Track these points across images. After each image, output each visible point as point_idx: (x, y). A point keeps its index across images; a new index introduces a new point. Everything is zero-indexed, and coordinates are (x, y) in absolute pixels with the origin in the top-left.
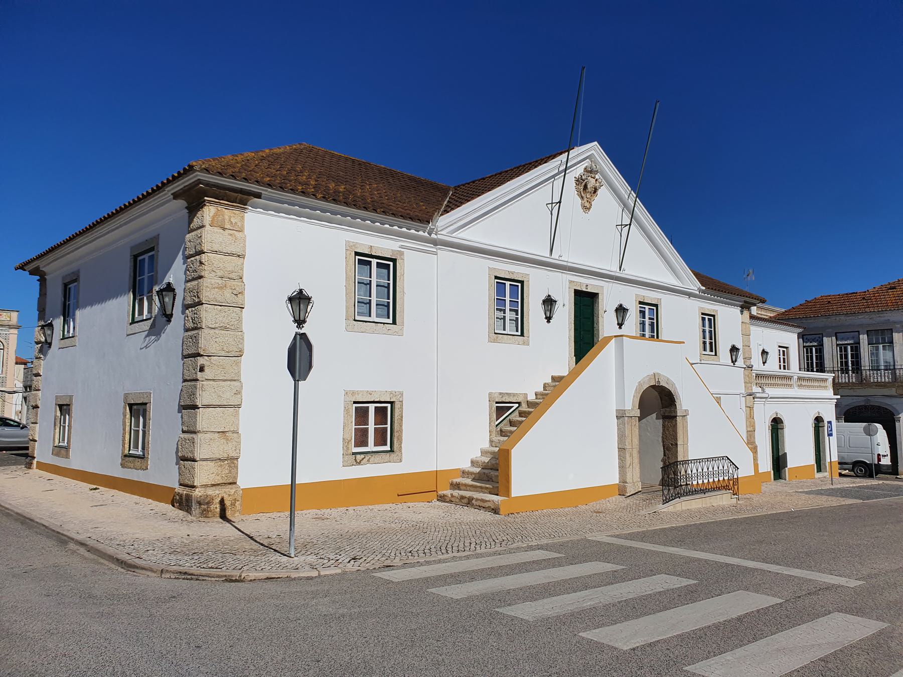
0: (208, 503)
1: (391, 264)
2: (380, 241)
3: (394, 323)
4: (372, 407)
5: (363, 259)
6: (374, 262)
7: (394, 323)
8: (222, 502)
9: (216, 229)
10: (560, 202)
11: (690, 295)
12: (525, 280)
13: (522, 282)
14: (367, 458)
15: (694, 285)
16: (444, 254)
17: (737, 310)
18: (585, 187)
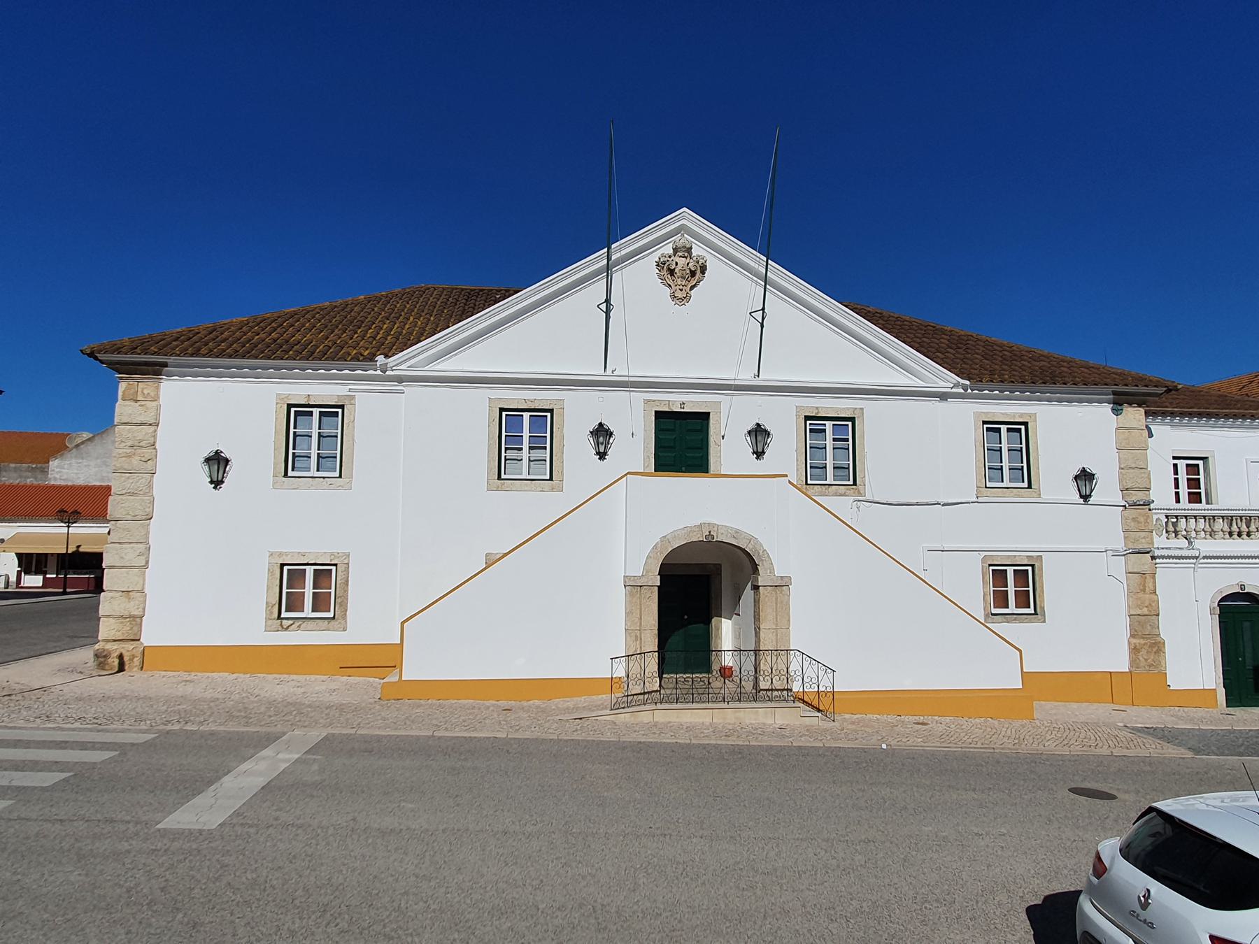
0: (105, 656)
1: (1023, 427)
3: (1030, 486)
4: (1010, 570)
5: (992, 427)
6: (1004, 428)
7: (1030, 486)
8: (121, 657)
9: (128, 403)
10: (763, 309)
11: (943, 397)
12: (555, 407)
14: (297, 624)
15: (946, 379)
18: (672, 272)
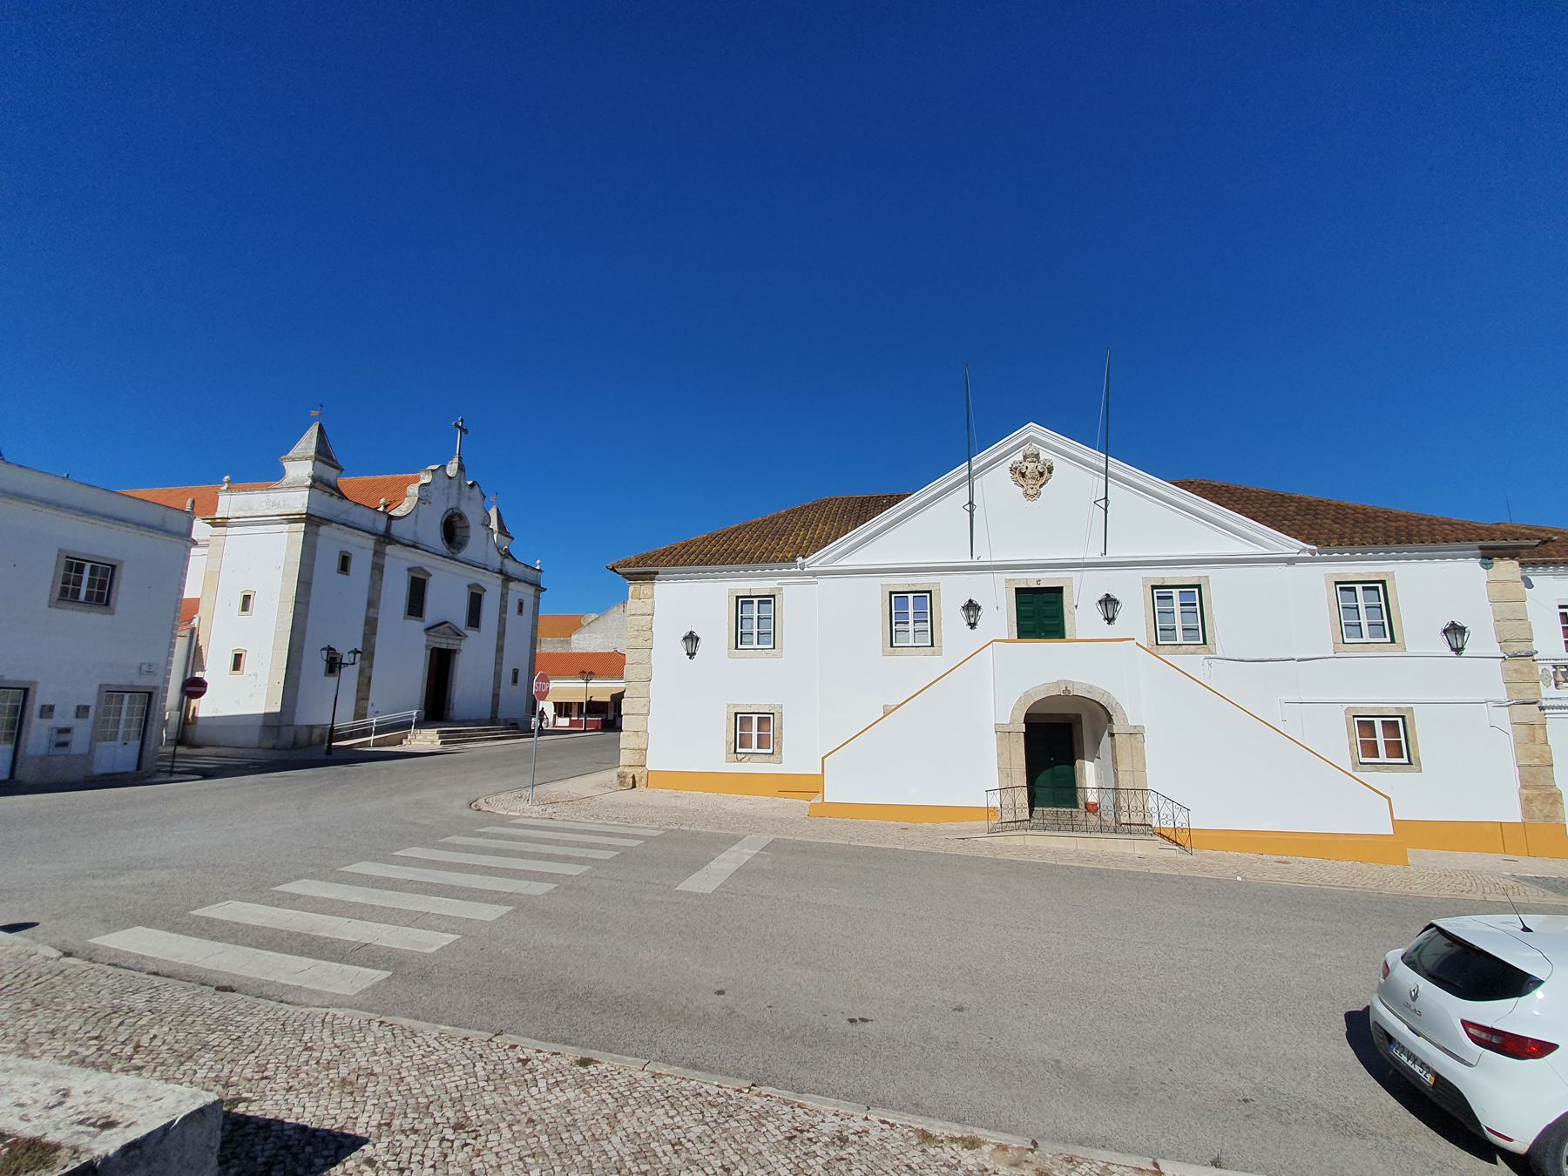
2: (755, 583)
3: (1393, 641)
4: (755, 717)
6: (1359, 587)
7: (1393, 641)
11: (1290, 561)
13: (1383, 582)
16: (823, 582)
17: (1474, 565)
18: (1023, 475)
